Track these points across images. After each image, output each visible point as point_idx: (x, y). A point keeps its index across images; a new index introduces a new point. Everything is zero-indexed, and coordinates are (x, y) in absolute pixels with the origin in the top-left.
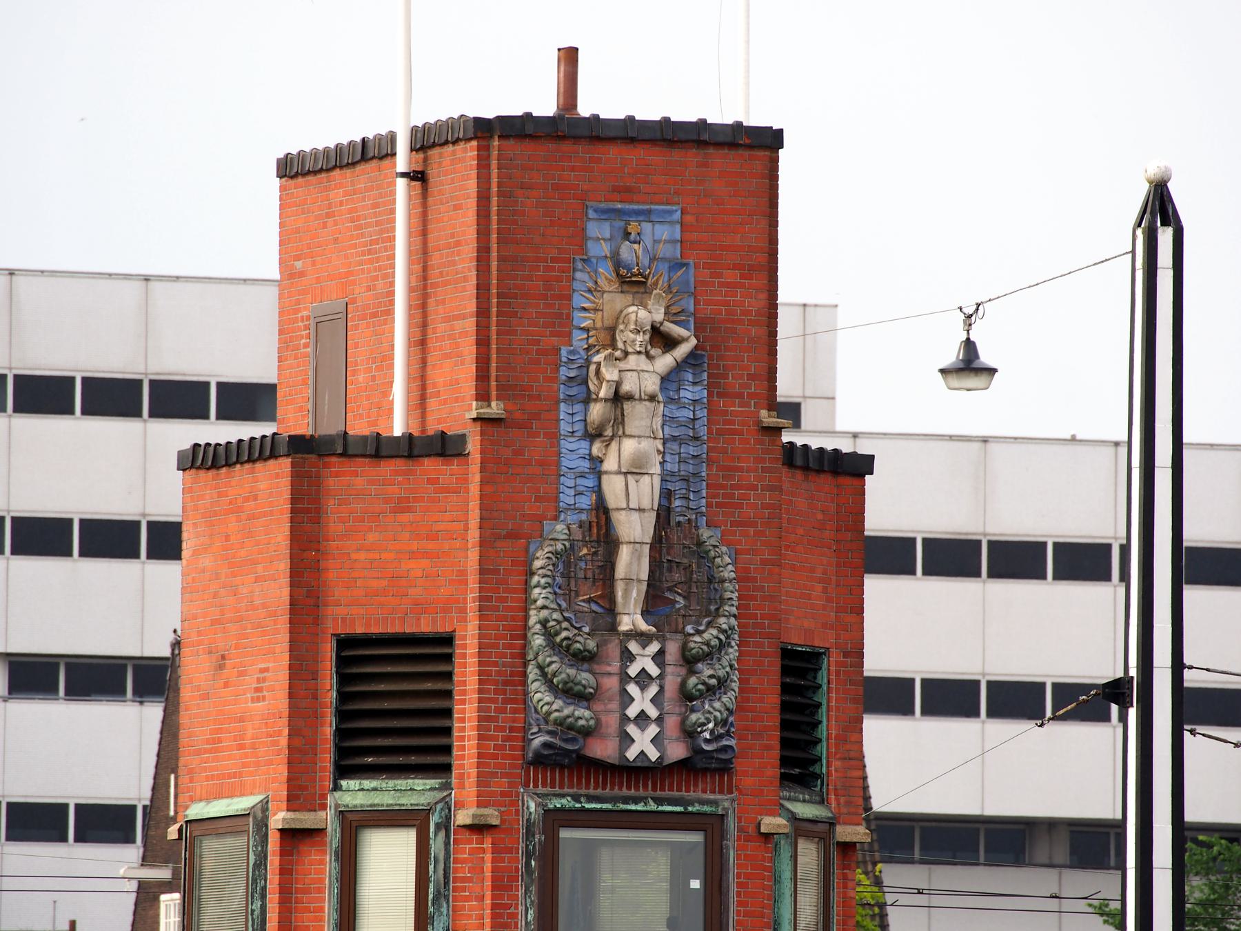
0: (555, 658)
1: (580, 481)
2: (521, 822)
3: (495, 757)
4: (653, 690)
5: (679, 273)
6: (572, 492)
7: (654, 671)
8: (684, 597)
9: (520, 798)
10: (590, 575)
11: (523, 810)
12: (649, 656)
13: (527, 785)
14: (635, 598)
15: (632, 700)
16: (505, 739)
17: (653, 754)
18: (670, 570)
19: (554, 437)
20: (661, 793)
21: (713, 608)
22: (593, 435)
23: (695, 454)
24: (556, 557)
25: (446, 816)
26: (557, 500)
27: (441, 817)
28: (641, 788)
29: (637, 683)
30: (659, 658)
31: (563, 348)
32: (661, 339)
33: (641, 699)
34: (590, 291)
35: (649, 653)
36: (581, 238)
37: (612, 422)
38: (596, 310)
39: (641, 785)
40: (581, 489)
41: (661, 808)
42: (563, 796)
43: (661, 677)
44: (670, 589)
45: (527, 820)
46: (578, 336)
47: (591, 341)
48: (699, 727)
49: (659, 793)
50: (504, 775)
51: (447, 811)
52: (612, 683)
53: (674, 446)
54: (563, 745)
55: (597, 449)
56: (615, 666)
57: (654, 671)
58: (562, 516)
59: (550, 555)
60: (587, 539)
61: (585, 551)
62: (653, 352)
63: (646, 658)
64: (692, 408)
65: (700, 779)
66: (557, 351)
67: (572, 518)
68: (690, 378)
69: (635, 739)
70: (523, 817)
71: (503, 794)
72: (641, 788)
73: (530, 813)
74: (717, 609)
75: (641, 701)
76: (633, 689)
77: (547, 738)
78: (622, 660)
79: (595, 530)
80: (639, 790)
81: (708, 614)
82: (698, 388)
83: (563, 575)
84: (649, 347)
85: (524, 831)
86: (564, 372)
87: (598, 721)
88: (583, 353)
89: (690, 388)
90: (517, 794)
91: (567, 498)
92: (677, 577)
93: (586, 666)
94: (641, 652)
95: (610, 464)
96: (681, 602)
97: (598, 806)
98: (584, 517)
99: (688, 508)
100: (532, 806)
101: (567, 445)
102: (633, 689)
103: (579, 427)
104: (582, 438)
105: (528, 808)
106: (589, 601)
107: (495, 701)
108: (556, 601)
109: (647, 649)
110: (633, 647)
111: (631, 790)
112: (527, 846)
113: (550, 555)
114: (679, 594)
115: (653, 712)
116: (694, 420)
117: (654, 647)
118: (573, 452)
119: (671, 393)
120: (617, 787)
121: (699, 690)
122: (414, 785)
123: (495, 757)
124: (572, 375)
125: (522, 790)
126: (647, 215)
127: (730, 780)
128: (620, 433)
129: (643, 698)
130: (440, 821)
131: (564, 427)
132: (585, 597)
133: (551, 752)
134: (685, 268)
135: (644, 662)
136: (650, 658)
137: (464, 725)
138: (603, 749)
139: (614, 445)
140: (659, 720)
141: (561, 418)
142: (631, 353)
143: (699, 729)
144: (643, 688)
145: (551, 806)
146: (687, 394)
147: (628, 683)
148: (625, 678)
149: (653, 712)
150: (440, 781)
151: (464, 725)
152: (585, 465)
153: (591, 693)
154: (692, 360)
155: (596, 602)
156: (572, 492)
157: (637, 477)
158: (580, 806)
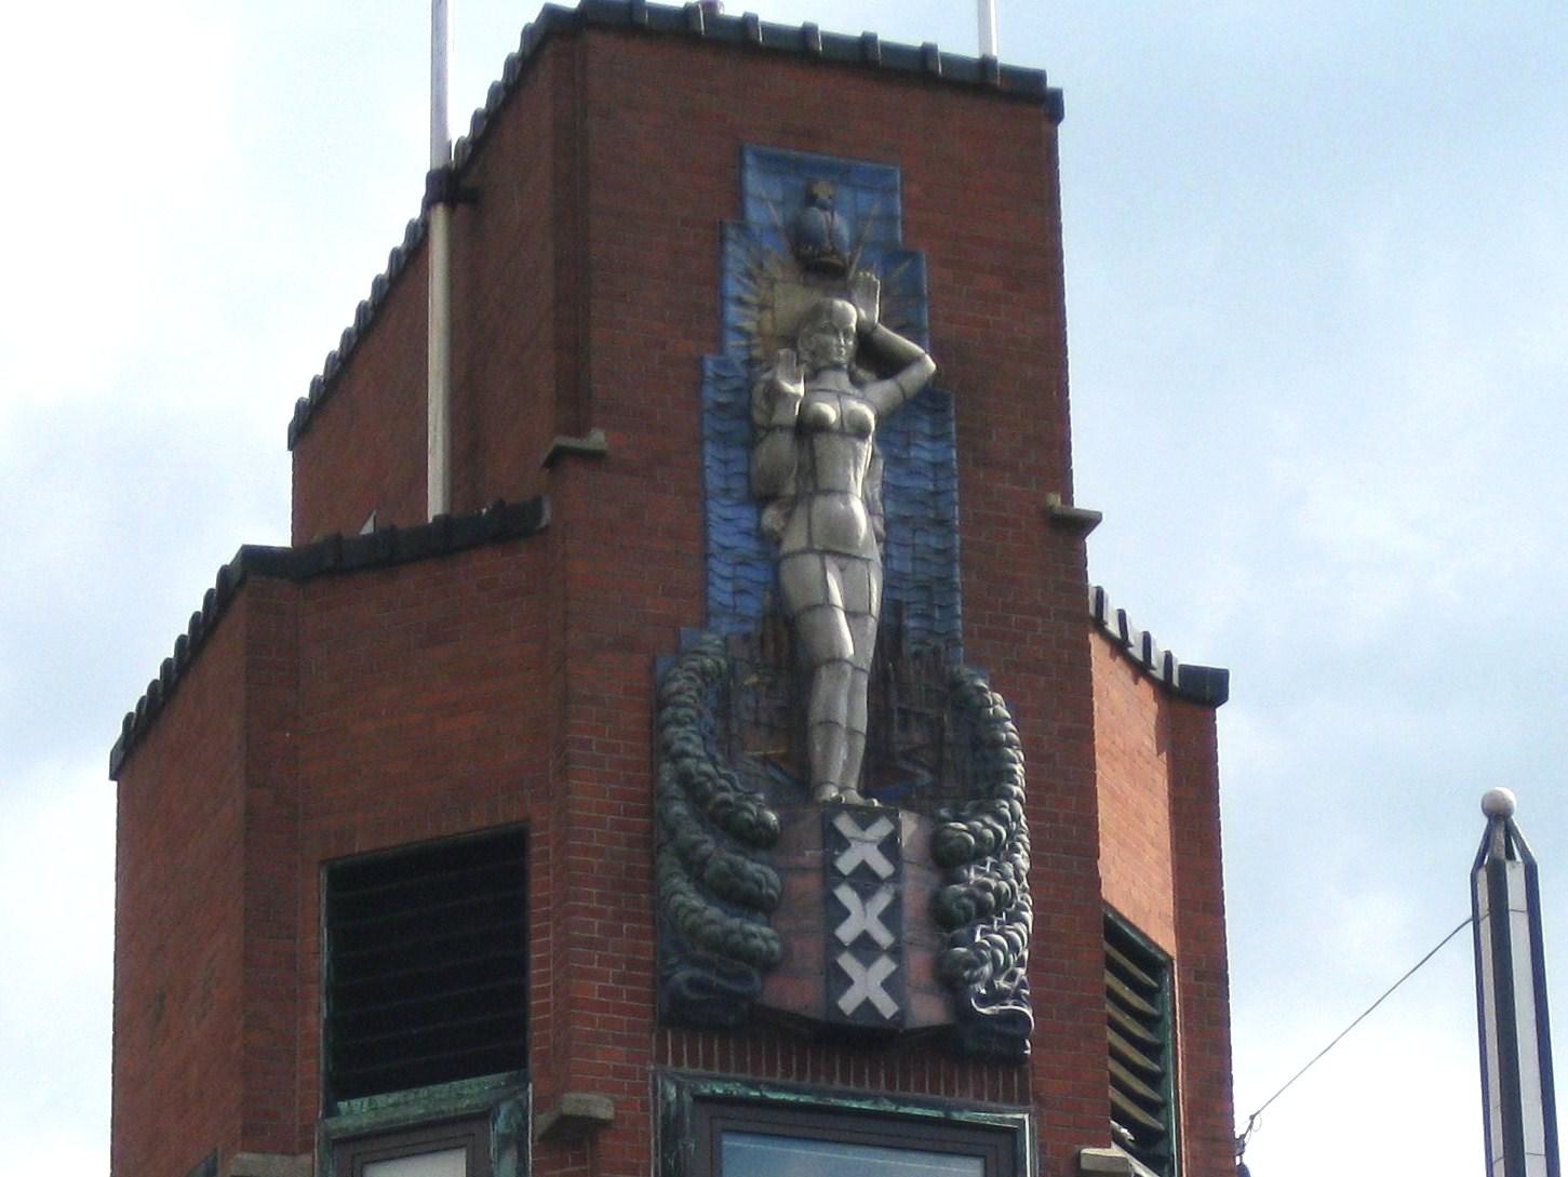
0: (708, 837)
1: (740, 571)
2: (652, 1122)
3: (603, 1007)
4: (882, 900)
5: (902, 269)
6: (729, 587)
7: (883, 867)
8: (931, 771)
9: (650, 1081)
10: (764, 718)
11: (656, 1101)
12: (872, 842)
13: (661, 1059)
14: (844, 761)
15: (850, 982)
16: (622, 979)
17: (887, 1007)
18: (904, 726)
19: (700, 496)
20: (902, 1093)
21: (982, 786)
22: (763, 498)
23: (940, 547)
24: (703, 680)
25: (519, 1125)
26: (705, 597)
27: (508, 1125)
28: (867, 1082)
29: (854, 887)
30: (890, 847)
31: (707, 356)
32: (875, 358)
33: (863, 913)
34: (750, 276)
35: (873, 838)
36: (737, 200)
37: (795, 471)
38: (762, 307)
39: (866, 1077)
40: (744, 584)
41: (902, 1110)
42: (728, 1080)
43: (896, 878)
44: (906, 756)
45: (663, 1118)
46: (733, 342)
47: (757, 353)
48: (967, 969)
49: (898, 1093)
50: (618, 1040)
51: (520, 1116)
52: (810, 884)
53: (905, 533)
54: (724, 983)
55: (771, 517)
56: (812, 855)
57: (883, 867)
58: (713, 622)
59: (692, 674)
60: (758, 660)
61: (754, 679)
62: (861, 373)
63: (868, 846)
64: (931, 475)
65: (971, 1079)
66: (698, 364)
67: (726, 626)
68: (926, 429)
69: (854, 978)
70: (656, 1112)
71: (619, 1072)
72: (867, 1082)
73: (669, 1104)
74: (991, 788)
75: (862, 918)
76: (846, 895)
77: (698, 973)
78: (824, 846)
79: (771, 647)
80: (864, 1084)
81: (976, 795)
82: (940, 445)
83: (715, 713)
84: (854, 366)
85: (659, 1137)
86: (711, 394)
87: (787, 951)
88: (743, 372)
89: (926, 444)
90: (644, 1076)
91: (721, 593)
92: (918, 737)
93: (763, 855)
94: (858, 833)
95: (795, 540)
96: (925, 778)
97: (792, 1098)
98: (750, 627)
99: (930, 632)
100: (672, 1091)
101: (718, 510)
102: (846, 895)
103: (738, 484)
104: (742, 503)
105: (664, 1096)
106: (765, 760)
107: (600, 914)
108: (720, 390)
109: (868, 830)
110: (844, 824)
111: (849, 1084)
112: (664, 1161)
113: (692, 674)
114: (923, 766)
115: (884, 938)
116: (936, 494)
117: (881, 828)
118: (727, 524)
119: (896, 450)
120: (823, 1078)
121: (965, 908)
122: (462, 1088)
123: (603, 1007)
124: (722, 399)
125: (652, 1067)
126: (843, 175)
127: (1024, 1079)
128: (810, 489)
129: (864, 910)
130: (507, 1131)
131: (714, 481)
132: (756, 754)
133: (704, 997)
134: (907, 264)
135: (863, 850)
136: (875, 847)
137: (546, 1000)
138: (794, 994)
139: (800, 513)
140: (895, 952)
141: (707, 463)
142: (825, 368)
143: (967, 973)
144: (865, 895)
145: (706, 1091)
146: (923, 453)
147: (836, 885)
148: (831, 876)
149: (884, 938)
150: (506, 1074)
151: (546, 1000)
152: (749, 546)
153: (771, 898)
154: (929, 399)
155: (773, 765)
156: (729, 587)
157: (844, 561)
158: (757, 1094)
